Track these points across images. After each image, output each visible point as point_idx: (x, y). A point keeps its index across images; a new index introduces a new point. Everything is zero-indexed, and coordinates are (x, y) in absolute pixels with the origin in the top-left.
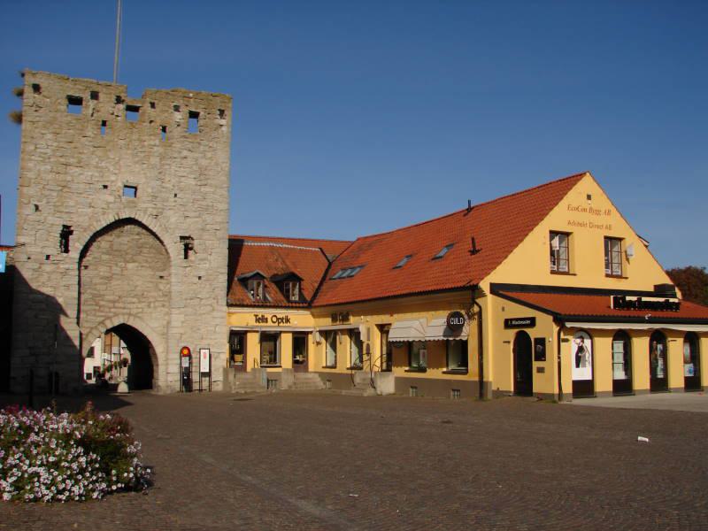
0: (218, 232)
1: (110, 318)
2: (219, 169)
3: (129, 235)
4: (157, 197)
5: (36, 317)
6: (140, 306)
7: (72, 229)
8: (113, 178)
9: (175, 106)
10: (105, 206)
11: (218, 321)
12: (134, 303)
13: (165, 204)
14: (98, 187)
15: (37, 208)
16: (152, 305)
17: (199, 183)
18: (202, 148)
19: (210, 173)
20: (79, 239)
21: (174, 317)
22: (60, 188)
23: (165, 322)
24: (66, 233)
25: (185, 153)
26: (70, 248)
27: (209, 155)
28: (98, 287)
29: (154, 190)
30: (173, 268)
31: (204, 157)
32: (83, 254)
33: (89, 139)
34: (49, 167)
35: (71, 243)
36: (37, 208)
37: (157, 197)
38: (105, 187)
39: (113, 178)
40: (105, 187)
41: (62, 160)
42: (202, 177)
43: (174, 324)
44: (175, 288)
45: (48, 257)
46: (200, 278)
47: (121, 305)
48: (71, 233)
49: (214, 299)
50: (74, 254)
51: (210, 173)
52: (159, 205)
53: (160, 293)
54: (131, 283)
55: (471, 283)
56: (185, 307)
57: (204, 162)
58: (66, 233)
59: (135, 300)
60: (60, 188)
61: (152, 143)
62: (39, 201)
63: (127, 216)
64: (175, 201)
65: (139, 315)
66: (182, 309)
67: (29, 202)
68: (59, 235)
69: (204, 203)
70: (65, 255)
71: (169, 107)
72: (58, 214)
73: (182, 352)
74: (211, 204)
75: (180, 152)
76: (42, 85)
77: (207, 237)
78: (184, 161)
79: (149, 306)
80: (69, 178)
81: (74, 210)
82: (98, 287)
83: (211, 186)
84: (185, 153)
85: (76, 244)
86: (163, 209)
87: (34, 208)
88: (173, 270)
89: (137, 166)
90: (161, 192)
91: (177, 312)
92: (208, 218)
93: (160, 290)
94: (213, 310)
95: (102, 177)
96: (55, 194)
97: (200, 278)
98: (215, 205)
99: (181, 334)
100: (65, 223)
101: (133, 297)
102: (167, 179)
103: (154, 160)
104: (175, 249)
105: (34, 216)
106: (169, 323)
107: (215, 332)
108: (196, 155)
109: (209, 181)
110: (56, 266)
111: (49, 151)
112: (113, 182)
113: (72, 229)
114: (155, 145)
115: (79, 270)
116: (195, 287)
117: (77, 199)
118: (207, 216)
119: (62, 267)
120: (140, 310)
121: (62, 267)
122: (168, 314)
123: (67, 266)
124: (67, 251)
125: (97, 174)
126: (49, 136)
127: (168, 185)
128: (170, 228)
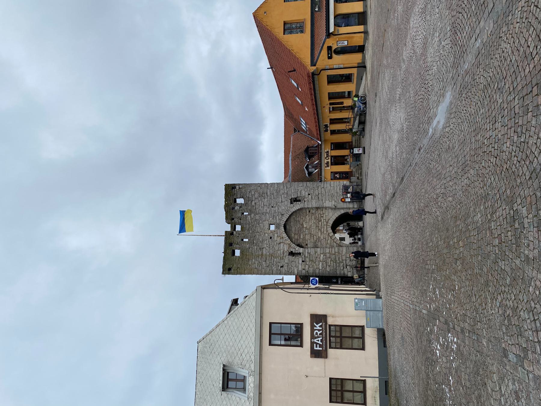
1: (329, 234)
3: (294, 228)
8: (267, 235)
11: (328, 185)
21: (327, 206)
24: (292, 254)
27: (253, 193)
35: (297, 252)
38: (271, 238)
39: (267, 235)
43: (330, 206)
46: (309, 194)
48: (292, 252)
57: (256, 195)
58: (292, 254)
59: (320, 223)
61: (250, 219)
82: (315, 239)
88: (306, 206)
92: (282, 192)
102: (265, 211)
103: (257, 217)
108: (254, 199)
124: (300, 254)
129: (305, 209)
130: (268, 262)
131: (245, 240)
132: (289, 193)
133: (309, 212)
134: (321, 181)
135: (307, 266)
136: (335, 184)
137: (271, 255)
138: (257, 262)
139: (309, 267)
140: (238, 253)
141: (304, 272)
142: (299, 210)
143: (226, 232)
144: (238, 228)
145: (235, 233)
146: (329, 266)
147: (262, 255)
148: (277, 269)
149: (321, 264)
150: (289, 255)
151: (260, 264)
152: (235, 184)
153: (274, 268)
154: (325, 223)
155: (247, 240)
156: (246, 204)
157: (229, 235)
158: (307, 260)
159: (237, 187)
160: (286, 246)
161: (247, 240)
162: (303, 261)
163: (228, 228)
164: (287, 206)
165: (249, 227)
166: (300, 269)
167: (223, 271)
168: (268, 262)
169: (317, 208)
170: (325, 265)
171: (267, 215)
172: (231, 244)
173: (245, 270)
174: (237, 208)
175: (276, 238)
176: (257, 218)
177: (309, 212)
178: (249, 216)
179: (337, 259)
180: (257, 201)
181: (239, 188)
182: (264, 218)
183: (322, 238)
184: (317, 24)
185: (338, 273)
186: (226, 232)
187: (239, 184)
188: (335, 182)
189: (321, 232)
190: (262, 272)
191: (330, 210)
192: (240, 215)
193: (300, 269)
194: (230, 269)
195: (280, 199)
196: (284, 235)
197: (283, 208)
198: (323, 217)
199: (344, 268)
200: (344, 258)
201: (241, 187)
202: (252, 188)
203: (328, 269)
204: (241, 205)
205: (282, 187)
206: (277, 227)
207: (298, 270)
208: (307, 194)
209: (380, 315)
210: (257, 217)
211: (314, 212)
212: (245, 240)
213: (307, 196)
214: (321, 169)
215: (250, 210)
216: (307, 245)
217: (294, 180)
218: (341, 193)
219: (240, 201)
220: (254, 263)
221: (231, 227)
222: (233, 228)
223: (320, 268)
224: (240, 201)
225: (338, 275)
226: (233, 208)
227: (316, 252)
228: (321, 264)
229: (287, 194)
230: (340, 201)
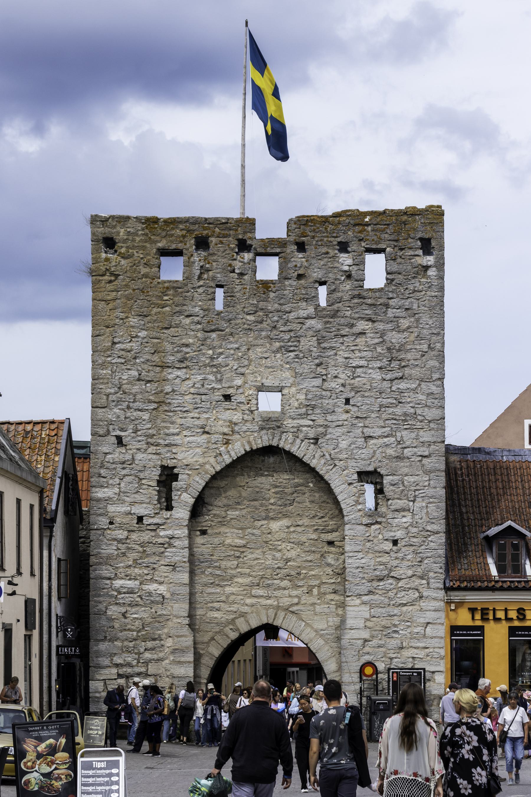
0: (425, 461)
1: (243, 615)
2: (425, 347)
3: (269, 483)
4: (314, 407)
5: (124, 615)
6: (294, 593)
7: (176, 471)
8: (239, 382)
9: (340, 243)
10: (226, 430)
11: (430, 616)
12: (285, 589)
13: (329, 418)
14: (217, 398)
15: (120, 441)
16: (315, 591)
17: (388, 377)
18: (391, 313)
19: (409, 356)
20: (189, 486)
21: (351, 612)
22: (154, 406)
23: (337, 620)
24: (168, 477)
25: (362, 325)
26: (174, 504)
27: (405, 323)
28: (224, 564)
29: (309, 397)
30: (347, 527)
31: (398, 329)
32: (196, 511)
33: (196, 319)
34: (135, 373)
35: (175, 495)
36: (120, 441)
37: (314, 407)
38: (227, 397)
39: (239, 382)
40: (227, 397)
41: (156, 358)
42: (394, 364)
43: (350, 622)
44: (351, 563)
45: (140, 519)
46: (395, 542)
47: (261, 592)
48: (175, 477)
49: (422, 578)
50: (181, 513)
51: (409, 356)
52: (321, 421)
53: (329, 570)
54: (278, 555)
55: (343, 695)
56: (370, 592)
57: (395, 338)
58: (168, 477)
59: (285, 583)
60: (154, 406)
61: (303, 313)
62: (122, 430)
63: (266, 443)
64: (347, 412)
65: (294, 608)
66: (365, 598)
67: (108, 433)
68: (154, 484)
69: (399, 410)
70: (166, 514)
71: (329, 244)
72: (152, 449)
73: (362, 671)
74: (412, 411)
75: (352, 326)
76: (117, 238)
77: (406, 470)
78: (361, 340)
79: (310, 592)
80: (168, 389)
81: (177, 439)
82: (224, 564)
83: (411, 378)
84: (362, 325)
85: (184, 500)
86: (326, 426)
87: (114, 440)
88: (348, 530)
89: (279, 355)
90: (321, 397)
91: (358, 602)
92: (407, 436)
93: (329, 565)
94: (421, 597)
95: (221, 380)
96: (146, 416)
97: (395, 542)
98: (419, 412)
99: (366, 641)
100: (165, 463)
101: (282, 579)
102: (333, 371)
103: (308, 343)
104: (330, 537)
105: (118, 454)
106: (343, 621)
107: (424, 636)
108: (381, 326)
109: (407, 371)
110: (153, 534)
111: (135, 345)
112: (239, 387)
113: (176, 471)
114: (308, 318)
115: (190, 537)
116: (385, 559)
117: (183, 421)
118: (405, 433)
119: (162, 533)
120: (296, 600)
121: (162, 533)
122: (342, 605)
123: (169, 532)
124: (169, 508)
125: (211, 377)
126: (133, 321)
127: (333, 385)
128: (339, 458)
129: (340, 526)
130: (136, 389)
131: (220, 293)
132: (403, 467)
133: (331, 543)
134: (447, 589)
135: (121, 534)
136: (435, 642)
137: (161, 403)
138: (135, 345)
139: (120, 541)
140: (173, 271)
141: (103, 522)
142: (337, 503)
143: (251, 222)
144: (268, 269)
145: (247, 256)
146: (124, 615)
147: (164, 366)
148: (110, 423)
149: (130, 584)
150: (164, 468)
151: (130, 359)
152: (442, 248)
153: (114, 413)
154: (286, 602)
155: (219, 305)
156: (360, 295)
157: (240, 235)
158: (146, 536)
159: (430, 260)
160: (197, 458)
161: (219, 305)
162: (140, 519)
163: (271, 226)
164: (351, 457)
165: (267, 313)
166: (111, 508)
167: (104, 221)
168: (136, 389)
169: (341, 573)
170: (128, 598)
171: (318, 382)
172: (202, 243)
173: (107, 302)
174: (346, 261)
175: (227, 415)
176: (303, 341)
177: (331, 543)
178: (311, 310)
179: (150, 644)
180: (372, 339)
181: (426, 268)
182: (307, 367)
183: (228, 590)
184: (47, 639)
185: (103, 646)
186: (251, 222)
187: (440, 265)
188: (442, 643)
189: (252, 585)
190: (103, 366)
191: (335, 621)
192: (317, 274)
193: (111, 508)
194: (109, 243)
195: (378, 432)
196: (238, 448)
197: (343, 444)
198: (309, 592)
199: (117, 665)
200: (152, 669)
201: (432, 272)
202: (425, 318)
203: (114, 611)
204: (354, 276)
205: (426, 436)
206: (271, 423)
207: (108, 500)
208: (399, 534)
209: (433, 580)
210: (308, 343)
211: (330, 559)
212: (220, 293)
213: (389, 535)
214: (493, 589)
215: (335, 314)
216: (204, 532)
217: (451, 473)
218: (397, 663)
219: (375, 271)
220: (134, 334)
221: (272, 241)
222: (270, 248)
223: (118, 583)
224: (375, 271)
225: (94, 647)
226: (344, 247)
227: (174, 567)
228: (130, 584)
229: (399, 458)
230: (367, 658)
